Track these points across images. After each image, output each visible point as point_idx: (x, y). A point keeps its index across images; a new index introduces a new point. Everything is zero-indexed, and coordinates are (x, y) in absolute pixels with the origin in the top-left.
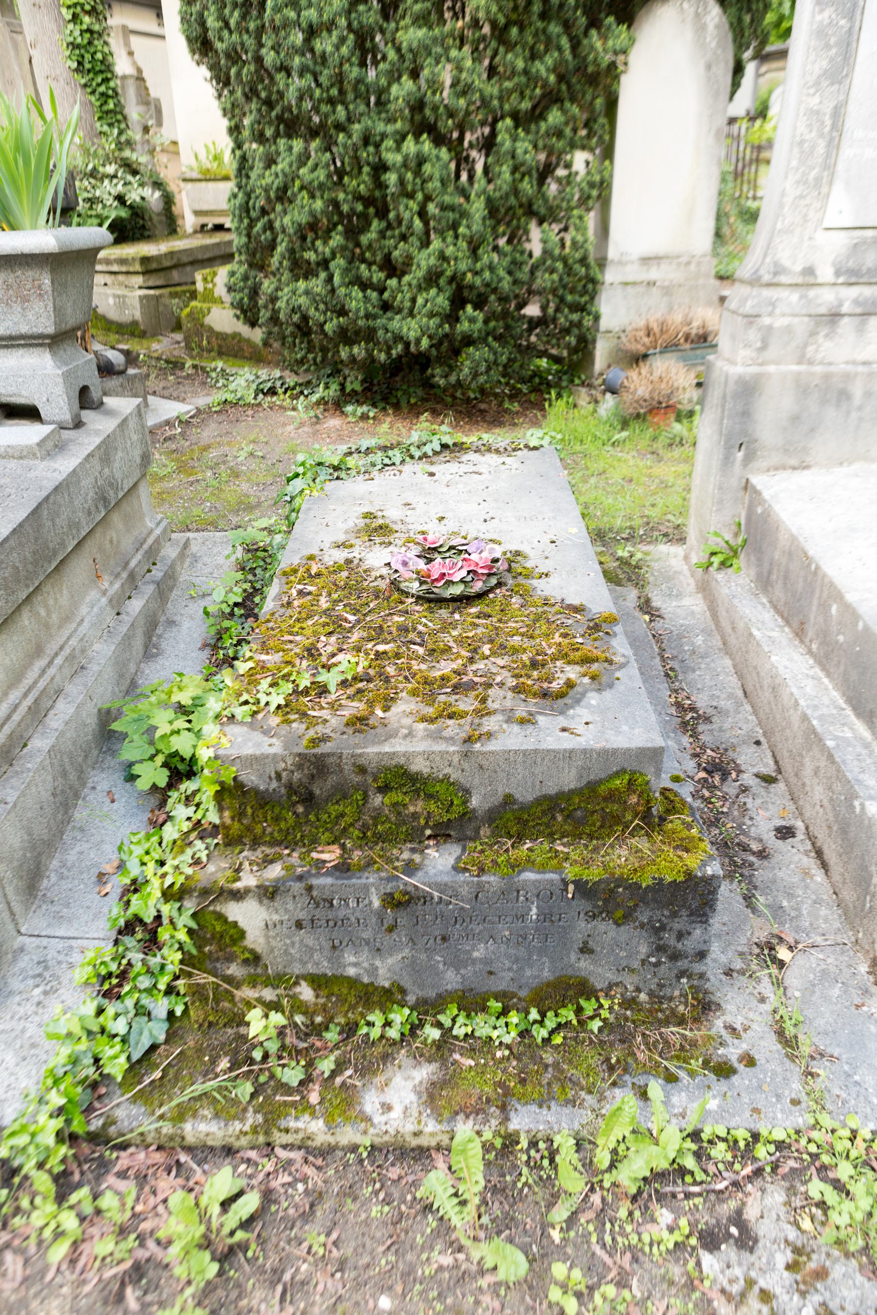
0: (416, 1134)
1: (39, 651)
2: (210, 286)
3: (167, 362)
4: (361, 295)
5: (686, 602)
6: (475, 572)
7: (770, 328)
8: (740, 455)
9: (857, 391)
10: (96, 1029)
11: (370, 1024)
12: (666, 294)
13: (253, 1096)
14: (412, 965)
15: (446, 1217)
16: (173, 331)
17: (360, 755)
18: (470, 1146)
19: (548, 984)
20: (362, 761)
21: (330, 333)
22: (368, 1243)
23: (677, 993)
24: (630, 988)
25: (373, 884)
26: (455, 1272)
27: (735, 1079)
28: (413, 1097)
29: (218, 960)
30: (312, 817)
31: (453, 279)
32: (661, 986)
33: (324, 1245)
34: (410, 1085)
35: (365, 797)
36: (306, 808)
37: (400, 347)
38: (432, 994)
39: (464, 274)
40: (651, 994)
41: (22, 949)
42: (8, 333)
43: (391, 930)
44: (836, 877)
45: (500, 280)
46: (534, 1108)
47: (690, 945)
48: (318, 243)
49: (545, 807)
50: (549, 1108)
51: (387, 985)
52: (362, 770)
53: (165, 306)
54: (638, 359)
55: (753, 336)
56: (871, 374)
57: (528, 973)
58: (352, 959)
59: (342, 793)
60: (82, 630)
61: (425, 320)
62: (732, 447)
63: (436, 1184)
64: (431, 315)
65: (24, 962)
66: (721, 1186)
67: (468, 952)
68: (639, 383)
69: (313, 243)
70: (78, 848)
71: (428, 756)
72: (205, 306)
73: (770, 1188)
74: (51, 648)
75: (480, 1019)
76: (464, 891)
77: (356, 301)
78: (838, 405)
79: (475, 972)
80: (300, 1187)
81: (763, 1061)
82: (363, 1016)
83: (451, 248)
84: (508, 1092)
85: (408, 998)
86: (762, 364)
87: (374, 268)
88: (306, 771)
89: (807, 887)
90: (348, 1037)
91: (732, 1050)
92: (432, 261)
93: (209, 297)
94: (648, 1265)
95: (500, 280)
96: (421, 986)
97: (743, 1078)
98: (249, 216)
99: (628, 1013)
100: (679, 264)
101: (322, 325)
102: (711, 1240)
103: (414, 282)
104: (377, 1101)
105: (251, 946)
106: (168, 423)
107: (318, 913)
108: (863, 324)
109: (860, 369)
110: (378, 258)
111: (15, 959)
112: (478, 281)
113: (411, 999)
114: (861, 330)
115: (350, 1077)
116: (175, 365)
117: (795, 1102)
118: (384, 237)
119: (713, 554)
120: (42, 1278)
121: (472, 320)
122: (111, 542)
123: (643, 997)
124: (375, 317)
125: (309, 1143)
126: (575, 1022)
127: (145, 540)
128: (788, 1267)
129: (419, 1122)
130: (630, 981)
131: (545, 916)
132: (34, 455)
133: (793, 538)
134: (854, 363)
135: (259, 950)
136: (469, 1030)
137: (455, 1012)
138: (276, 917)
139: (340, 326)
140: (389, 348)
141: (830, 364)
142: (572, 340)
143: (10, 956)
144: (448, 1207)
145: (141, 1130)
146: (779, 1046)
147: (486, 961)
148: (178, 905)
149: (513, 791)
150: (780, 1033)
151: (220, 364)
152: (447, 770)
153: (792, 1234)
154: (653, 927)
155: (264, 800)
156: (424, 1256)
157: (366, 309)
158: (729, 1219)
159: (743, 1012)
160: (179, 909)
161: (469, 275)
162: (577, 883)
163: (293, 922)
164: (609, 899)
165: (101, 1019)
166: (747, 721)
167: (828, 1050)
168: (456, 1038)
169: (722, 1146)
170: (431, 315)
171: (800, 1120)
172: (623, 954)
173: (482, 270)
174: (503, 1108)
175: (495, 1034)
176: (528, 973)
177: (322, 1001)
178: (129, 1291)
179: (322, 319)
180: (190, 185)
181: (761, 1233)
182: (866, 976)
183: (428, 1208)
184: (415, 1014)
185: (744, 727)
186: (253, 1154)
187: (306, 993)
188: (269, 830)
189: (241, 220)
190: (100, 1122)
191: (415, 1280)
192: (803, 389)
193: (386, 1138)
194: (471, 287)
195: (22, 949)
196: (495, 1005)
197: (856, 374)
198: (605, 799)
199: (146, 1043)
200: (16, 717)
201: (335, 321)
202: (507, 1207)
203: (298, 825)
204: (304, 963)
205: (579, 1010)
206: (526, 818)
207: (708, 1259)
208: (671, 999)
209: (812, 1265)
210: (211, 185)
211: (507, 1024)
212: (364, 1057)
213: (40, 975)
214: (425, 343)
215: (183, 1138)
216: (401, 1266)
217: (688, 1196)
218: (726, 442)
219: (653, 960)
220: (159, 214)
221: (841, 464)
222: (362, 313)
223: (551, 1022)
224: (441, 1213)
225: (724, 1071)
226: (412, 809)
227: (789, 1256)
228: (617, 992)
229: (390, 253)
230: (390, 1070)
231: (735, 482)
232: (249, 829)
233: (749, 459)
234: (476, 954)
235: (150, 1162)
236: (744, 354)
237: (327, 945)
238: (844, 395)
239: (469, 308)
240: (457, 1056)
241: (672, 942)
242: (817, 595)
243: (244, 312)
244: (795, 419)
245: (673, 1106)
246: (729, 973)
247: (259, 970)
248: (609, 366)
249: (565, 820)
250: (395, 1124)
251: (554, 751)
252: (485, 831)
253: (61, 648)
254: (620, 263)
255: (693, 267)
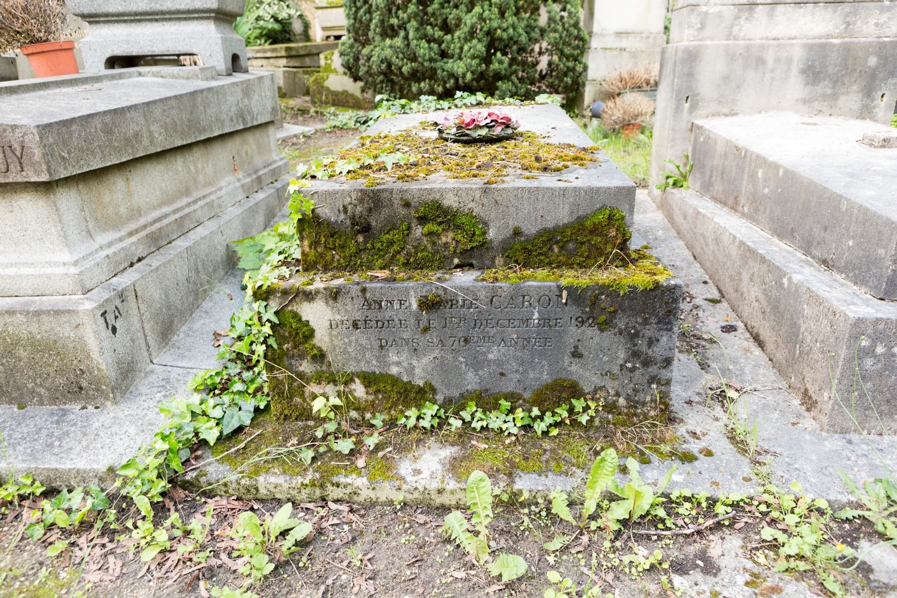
0: (440, 492)
1: (187, 192)
2: (329, 62)
3: (299, 110)
4: (426, 45)
5: (650, 215)
6: (496, 121)
7: (706, 14)
8: (687, 105)
9: (770, 57)
10: (198, 411)
11: (407, 418)
12: (633, 57)
13: (314, 459)
14: (441, 366)
15: (462, 546)
16: (304, 95)
17: (406, 191)
18: (482, 484)
19: (547, 387)
20: (408, 197)
21: (406, 73)
22: (397, 561)
23: (648, 398)
24: (612, 392)
25: (412, 288)
26: (466, 583)
27: (696, 463)
28: (439, 467)
29: (293, 357)
30: (369, 245)
31: (488, 33)
32: (636, 391)
33: (361, 561)
34: (437, 459)
35: (409, 228)
36: (365, 238)
37: (452, 81)
38: (456, 393)
39: (496, 30)
40: (628, 399)
41: (152, 372)
42: (187, 8)
43: (426, 330)
44: (770, 346)
45: (520, 35)
46: (535, 476)
47: (658, 351)
48: (400, 12)
49: (545, 238)
50: (547, 476)
51: (421, 383)
52: (407, 205)
53: (300, 79)
54: (611, 96)
55: (695, 20)
56: (779, 46)
57: (531, 376)
58: (395, 359)
59: (391, 226)
60: (219, 194)
61: (469, 60)
62: (681, 99)
63: (455, 522)
64: (473, 57)
65: (151, 379)
66: (688, 532)
67: (484, 354)
68: (615, 110)
69: (396, 13)
70: (202, 322)
71: (457, 192)
72: (325, 74)
73: (728, 537)
74: (196, 195)
75: (493, 415)
76: (482, 295)
77: (423, 49)
78: (756, 69)
79: (490, 374)
80: (346, 527)
81: (719, 454)
82: (402, 412)
83: (487, 12)
84: (514, 465)
85: (437, 397)
86: (701, 40)
87: (436, 28)
88: (366, 205)
89: (747, 358)
90: (390, 428)
91: (693, 445)
92: (475, 20)
93: (328, 69)
94: (628, 582)
95: (520, 35)
96: (448, 386)
97: (703, 463)
98: (356, 6)
99: (610, 416)
100: (642, 38)
101: (400, 68)
102: (680, 568)
103: (463, 36)
104: (410, 468)
105: (319, 344)
106: (295, 136)
107: (371, 314)
108: (773, 10)
109: (772, 42)
110: (439, 22)
111: (146, 376)
112: (505, 36)
113: (440, 397)
114: (771, 15)
115: (390, 452)
116: (304, 112)
117: (747, 480)
118: (443, 8)
119: (668, 177)
120: (136, 574)
121: (501, 62)
122: (247, 153)
123: (622, 401)
124: (435, 61)
125: (355, 498)
126: (568, 422)
127: (271, 164)
128: (747, 584)
129: (443, 482)
130: (611, 387)
131: (545, 321)
132: (197, 76)
133: (728, 142)
134: (767, 39)
135: (325, 349)
136: (484, 424)
137: (474, 409)
138: (338, 317)
139: (412, 68)
140: (445, 83)
141: (750, 39)
142: (568, 80)
143: (143, 374)
144: (465, 540)
145: (225, 480)
146: (732, 446)
147: (498, 363)
148: (265, 303)
149: (521, 225)
150: (732, 439)
151: (333, 109)
152: (471, 205)
153: (749, 565)
154: (629, 333)
155: (333, 230)
156: (442, 571)
157: (430, 54)
158: (695, 556)
159: (700, 425)
160: (266, 307)
161: (499, 31)
162: (569, 289)
163: (351, 322)
164: (595, 307)
165: (203, 406)
166: (697, 272)
167: (772, 449)
168: (474, 429)
169: (688, 505)
170: (473, 57)
171: (752, 491)
172: (606, 359)
173: (508, 28)
174: (510, 475)
175: (504, 427)
176: (531, 376)
177: (371, 398)
178: (202, 583)
179: (400, 63)
180: (320, 11)
181: (722, 565)
182: (799, 407)
183: (448, 541)
184: (443, 411)
185: (695, 275)
186: (311, 506)
187: (359, 390)
188: (337, 257)
189: (350, 9)
190: (194, 474)
191: (433, 587)
192: (731, 57)
193: (416, 495)
194: (501, 39)
195: (152, 372)
196: (505, 404)
197: (769, 45)
198: (591, 232)
199: (235, 424)
200: (165, 222)
201: (409, 65)
202: (511, 543)
203: (359, 252)
204: (358, 362)
205: (571, 411)
206: (528, 250)
207: (677, 580)
208: (644, 404)
209: (769, 583)
210: (334, 10)
211: (514, 419)
212: (402, 440)
213: (162, 386)
214: (469, 76)
215: (257, 489)
216: (422, 576)
217: (660, 538)
218: (677, 96)
219: (629, 365)
220: (300, 35)
221: (760, 112)
222: (427, 57)
223: (549, 419)
224: (458, 542)
225: (688, 458)
226: (444, 239)
227: (748, 577)
228: (601, 394)
229: (447, 18)
230: (421, 449)
231: (684, 125)
232: (321, 256)
233: (693, 108)
234: (491, 356)
235: (230, 506)
236: (688, 32)
237: (376, 344)
238: (760, 61)
239: (499, 54)
240: (474, 442)
241: (644, 348)
242: (746, 171)
243: (349, 69)
244: (726, 78)
245: (647, 478)
246: (689, 402)
247: (324, 368)
248: (594, 101)
249: (560, 252)
250: (423, 482)
251: (551, 189)
252: (499, 261)
253: (204, 197)
254: (602, 35)
255: (651, 40)
